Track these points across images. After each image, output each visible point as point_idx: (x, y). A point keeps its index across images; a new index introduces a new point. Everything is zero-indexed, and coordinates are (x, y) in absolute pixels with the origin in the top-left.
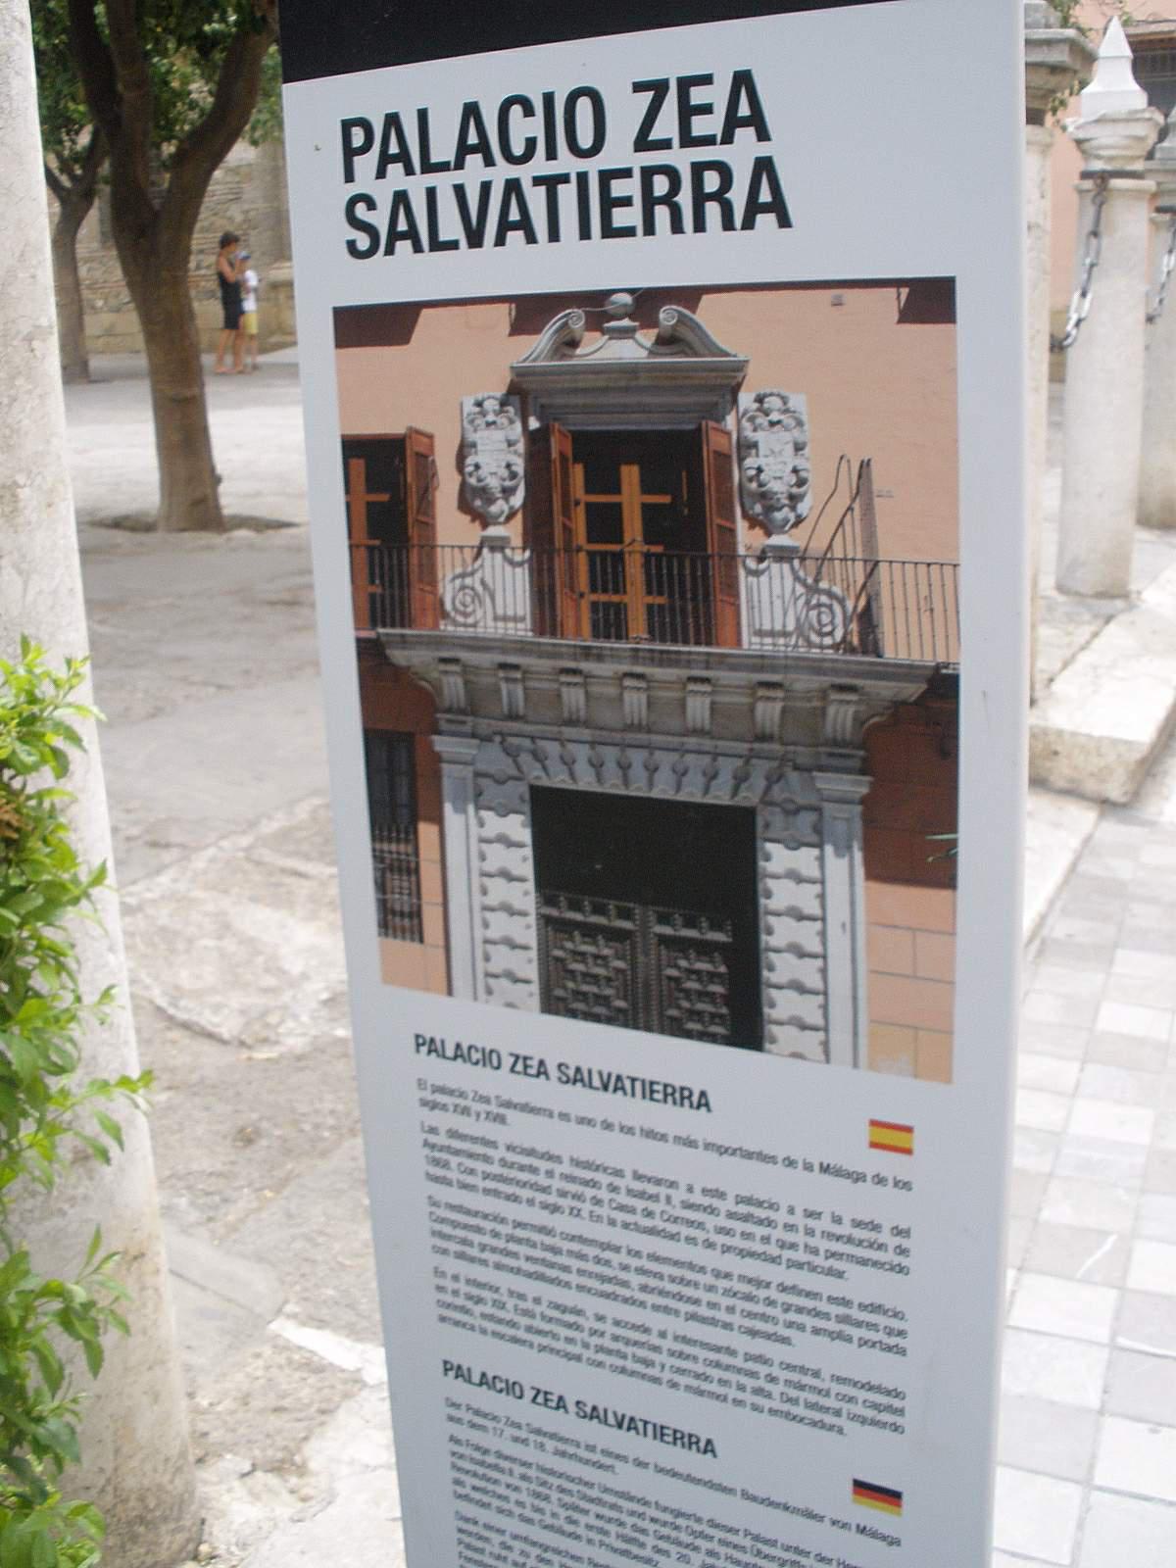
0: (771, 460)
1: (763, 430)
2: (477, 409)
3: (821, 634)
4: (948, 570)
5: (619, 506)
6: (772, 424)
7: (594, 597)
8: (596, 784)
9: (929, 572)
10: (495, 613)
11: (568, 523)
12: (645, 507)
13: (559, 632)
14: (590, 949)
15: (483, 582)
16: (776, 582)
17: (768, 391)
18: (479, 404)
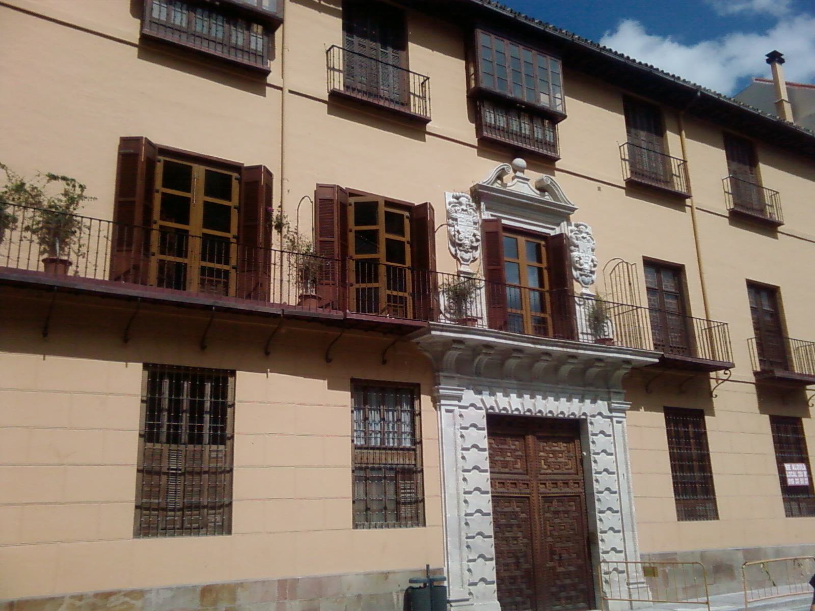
0: (584, 255)
1: (580, 240)
2: (455, 200)
4: (725, 326)
5: (188, 200)
6: (463, 210)
7: (357, 286)
8: (608, 412)
12: (206, 204)
13: (182, 287)
17: (581, 223)
18: (457, 198)
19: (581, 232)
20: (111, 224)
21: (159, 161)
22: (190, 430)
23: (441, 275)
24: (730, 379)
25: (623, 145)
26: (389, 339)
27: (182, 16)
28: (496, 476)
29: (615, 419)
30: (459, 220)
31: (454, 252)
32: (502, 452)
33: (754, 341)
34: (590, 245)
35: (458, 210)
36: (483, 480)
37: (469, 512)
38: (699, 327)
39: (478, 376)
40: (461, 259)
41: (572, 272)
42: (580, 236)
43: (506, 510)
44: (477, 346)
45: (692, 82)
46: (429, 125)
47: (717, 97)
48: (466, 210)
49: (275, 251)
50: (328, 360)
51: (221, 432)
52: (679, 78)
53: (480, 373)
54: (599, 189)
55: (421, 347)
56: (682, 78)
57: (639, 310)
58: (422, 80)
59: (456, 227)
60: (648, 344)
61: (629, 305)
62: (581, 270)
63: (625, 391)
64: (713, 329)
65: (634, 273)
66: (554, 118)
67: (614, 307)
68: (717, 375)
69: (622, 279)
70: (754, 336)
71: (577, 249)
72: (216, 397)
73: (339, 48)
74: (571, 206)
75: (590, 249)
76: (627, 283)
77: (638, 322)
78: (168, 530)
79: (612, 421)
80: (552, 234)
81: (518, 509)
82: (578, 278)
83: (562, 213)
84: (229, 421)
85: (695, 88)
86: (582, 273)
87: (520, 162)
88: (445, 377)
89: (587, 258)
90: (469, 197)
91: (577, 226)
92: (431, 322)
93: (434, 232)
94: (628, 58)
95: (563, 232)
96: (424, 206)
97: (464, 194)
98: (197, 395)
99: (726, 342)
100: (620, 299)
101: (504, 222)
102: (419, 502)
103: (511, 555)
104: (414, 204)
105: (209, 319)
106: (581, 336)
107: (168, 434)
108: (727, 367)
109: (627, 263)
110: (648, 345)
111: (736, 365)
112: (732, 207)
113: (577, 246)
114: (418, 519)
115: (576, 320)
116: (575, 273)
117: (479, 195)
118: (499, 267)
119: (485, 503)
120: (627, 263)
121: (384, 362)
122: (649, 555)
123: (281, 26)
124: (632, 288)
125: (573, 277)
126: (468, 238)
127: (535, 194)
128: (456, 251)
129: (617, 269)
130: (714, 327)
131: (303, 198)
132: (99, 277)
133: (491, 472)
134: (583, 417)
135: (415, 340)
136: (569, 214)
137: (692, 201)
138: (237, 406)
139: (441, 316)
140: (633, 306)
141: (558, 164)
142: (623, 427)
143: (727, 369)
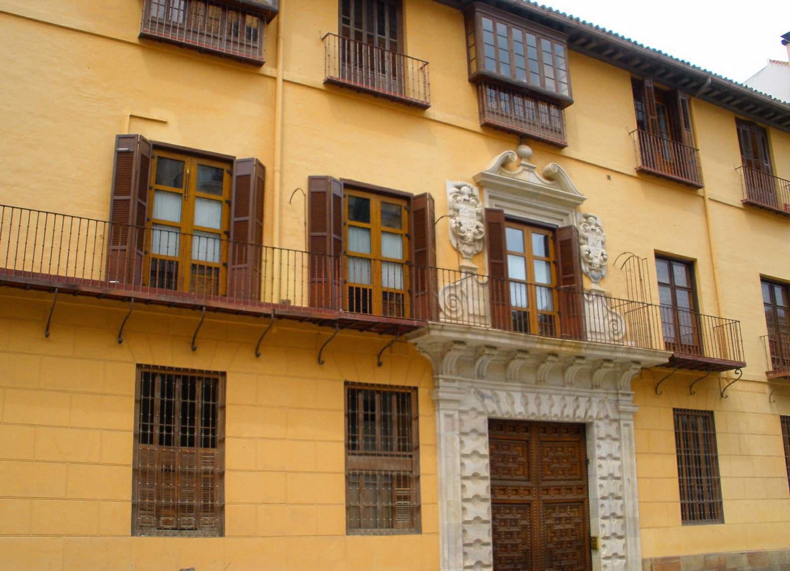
1: (590, 232)
2: (458, 190)
3: (451, 311)
4: (737, 323)
9: (288, 254)
10: (468, 312)
11: (143, 203)
14: (563, 515)
15: (462, 292)
16: (595, 305)
17: (592, 214)
19: (590, 224)
20: (107, 224)
21: (153, 157)
22: (182, 433)
23: (442, 270)
24: (742, 378)
25: (633, 132)
26: (387, 338)
27: (179, 13)
28: (498, 483)
29: (622, 423)
30: (460, 211)
31: (455, 246)
32: (504, 458)
33: (767, 338)
34: (600, 238)
35: (461, 200)
36: (483, 488)
37: (467, 519)
38: (708, 326)
39: (480, 379)
40: (463, 253)
41: (580, 266)
42: (589, 228)
43: (507, 517)
44: (480, 347)
45: (703, 68)
46: (428, 110)
47: (728, 83)
48: (469, 200)
49: (266, 247)
50: (320, 362)
51: (212, 435)
52: (688, 64)
53: (482, 376)
54: (609, 178)
55: (419, 348)
56: (692, 64)
57: (650, 307)
58: (421, 64)
59: (457, 218)
60: (659, 343)
61: (640, 303)
62: (590, 264)
63: (634, 393)
64: (725, 326)
65: (645, 268)
66: (560, 103)
67: (643, 307)
68: (727, 374)
69: (633, 274)
70: (766, 333)
71: (585, 242)
72: (207, 399)
73: (335, 35)
74: (579, 196)
75: (600, 242)
76: (638, 279)
77: (649, 320)
78: (161, 529)
79: (619, 424)
80: (560, 226)
81: (518, 516)
82: (588, 273)
83: (574, 203)
84: (219, 424)
85: (706, 74)
86: (592, 268)
87: (526, 149)
88: (446, 380)
89: (597, 252)
90: (472, 186)
91: (586, 217)
92: (429, 322)
93: (434, 223)
94: (635, 43)
95: (571, 224)
96: (423, 196)
97: (465, 183)
98: (189, 397)
99: (738, 341)
100: (635, 296)
101: (507, 212)
102: (416, 510)
103: (509, 561)
104: (412, 194)
105: (337, 334)
106: (589, 335)
107: (161, 436)
108: (739, 366)
109: (638, 258)
110: (658, 344)
111: (747, 364)
112: (746, 197)
113: (586, 239)
114: (415, 526)
115: (585, 318)
116: (585, 268)
117: (483, 182)
118: (501, 262)
119: (484, 510)
120: (638, 258)
121: (380, 364)
122: (651, 559)
123: (276, 16)
124: (643, 284)
125: (582, 272)
126: (470, 230)
127: (540, 183)
128: (457, 244)
129: (627, 263)
130: (726, 324)
131: (296, 191)
132: (96, 278)
133: (492, 479)
134: (590, 420)
135: (413, 341)
136: (579, 204)
137: (704, 192)
138: (228, 409)
139: (441, 315)
140: (643, 303)
141: (566, 151)
142: (630, 431)
143: (738, 368)
